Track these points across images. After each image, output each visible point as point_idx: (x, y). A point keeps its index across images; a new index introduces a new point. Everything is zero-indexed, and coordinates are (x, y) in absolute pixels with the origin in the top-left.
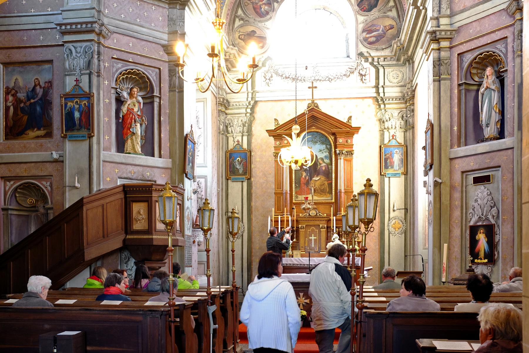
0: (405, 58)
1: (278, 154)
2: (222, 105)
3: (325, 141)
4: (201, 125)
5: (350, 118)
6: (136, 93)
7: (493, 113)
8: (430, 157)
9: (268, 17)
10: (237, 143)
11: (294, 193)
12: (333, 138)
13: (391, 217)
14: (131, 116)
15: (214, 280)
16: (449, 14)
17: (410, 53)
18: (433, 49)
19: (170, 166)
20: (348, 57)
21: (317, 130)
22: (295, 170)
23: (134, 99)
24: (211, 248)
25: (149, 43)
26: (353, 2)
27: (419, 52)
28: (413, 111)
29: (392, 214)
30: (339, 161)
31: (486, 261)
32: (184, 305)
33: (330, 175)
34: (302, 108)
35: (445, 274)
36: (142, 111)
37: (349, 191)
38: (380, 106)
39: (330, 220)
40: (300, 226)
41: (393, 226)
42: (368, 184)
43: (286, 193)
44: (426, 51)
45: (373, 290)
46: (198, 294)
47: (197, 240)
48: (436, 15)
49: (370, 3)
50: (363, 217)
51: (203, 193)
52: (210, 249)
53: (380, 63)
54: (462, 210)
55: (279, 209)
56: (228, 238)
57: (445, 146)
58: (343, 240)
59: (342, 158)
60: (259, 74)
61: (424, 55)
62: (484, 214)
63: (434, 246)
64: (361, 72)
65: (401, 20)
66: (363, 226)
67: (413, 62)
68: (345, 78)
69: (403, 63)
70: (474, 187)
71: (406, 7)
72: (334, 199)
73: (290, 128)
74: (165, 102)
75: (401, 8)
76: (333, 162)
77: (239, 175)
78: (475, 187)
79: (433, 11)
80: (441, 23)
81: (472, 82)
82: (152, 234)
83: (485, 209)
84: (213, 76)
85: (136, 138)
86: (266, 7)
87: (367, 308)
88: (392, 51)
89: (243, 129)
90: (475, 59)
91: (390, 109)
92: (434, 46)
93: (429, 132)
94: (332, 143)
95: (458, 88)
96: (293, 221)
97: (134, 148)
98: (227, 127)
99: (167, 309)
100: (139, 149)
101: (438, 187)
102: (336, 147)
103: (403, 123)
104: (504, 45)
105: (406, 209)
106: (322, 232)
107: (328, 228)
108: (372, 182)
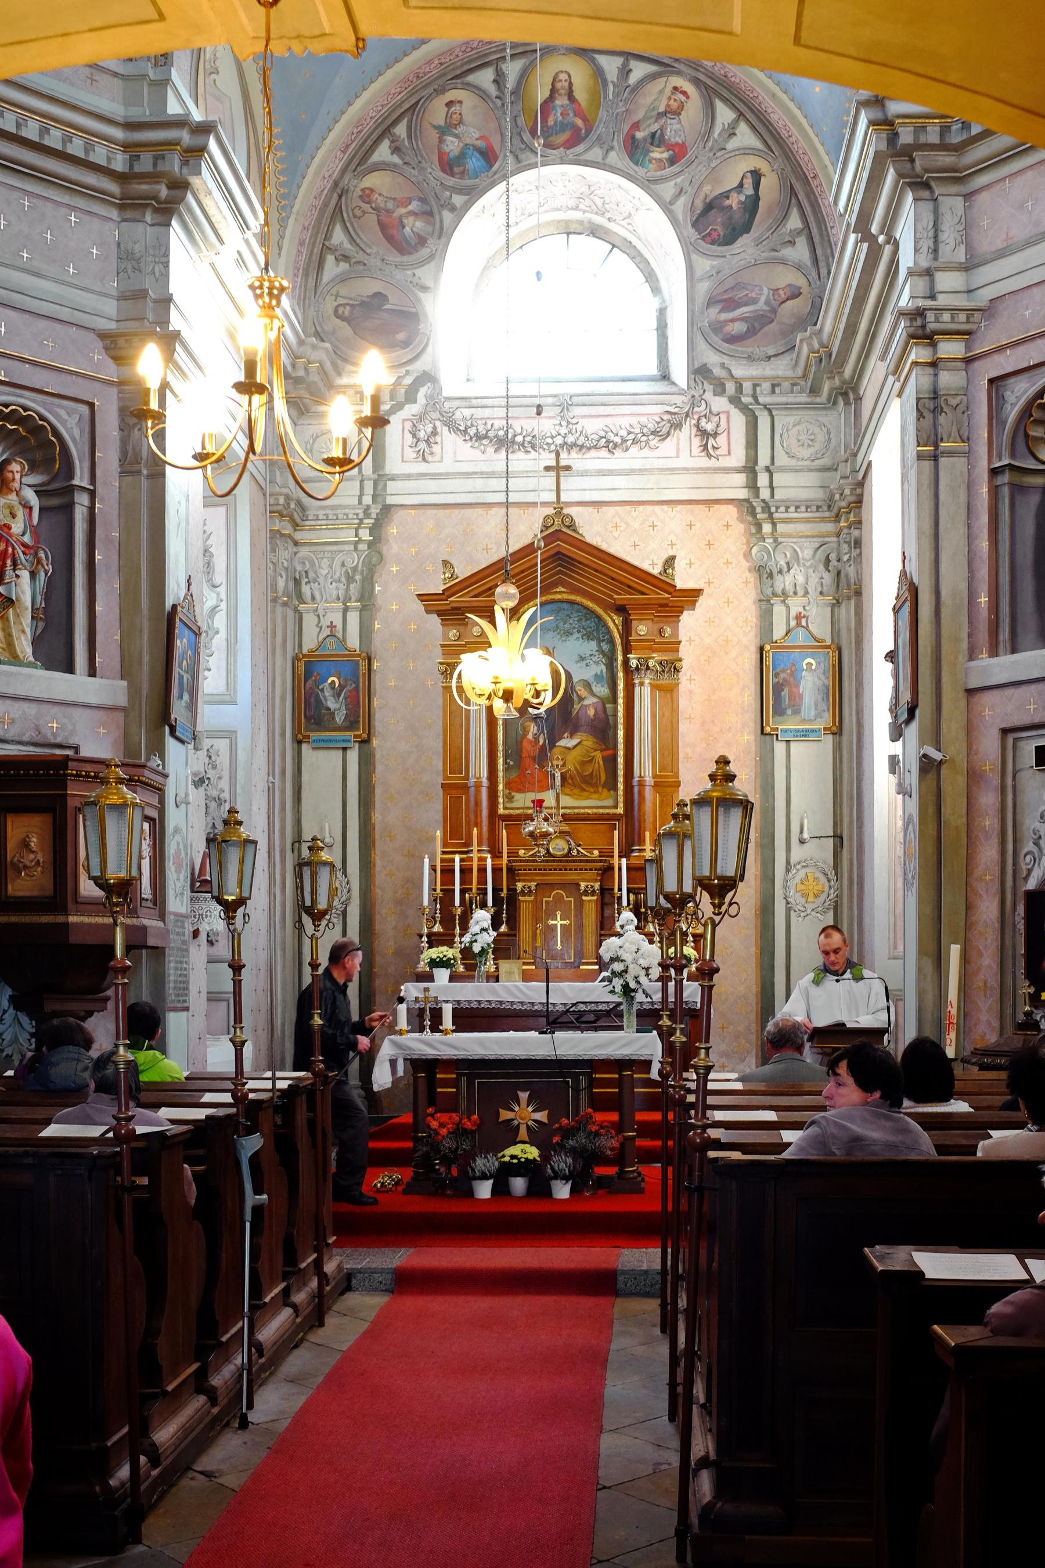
1: (453, 666)
2: (282, 516)
3: (597, 631)
4: (220, 577)
5: (670, 561)
6: (17, 476)
8: (908, 685)
9: (425, 252)
10: (328, 632)
11: (501, 787)
12: (618, 620)
13: (793, 862)
15: (257, 1050)
16: (963, 260)
18: (915, 364)
19: (122, 700)
21: (573, 597)
22: (505, 721)
23: (13, 497)
24: (245, 959)
25: (58, 326)
26: (681, 218)
27: (876, 370)
28: (858, 543)
29: (798, 853)
30: (637, 689)
32: (162, 1134)
33: (611, 733)
34: (527, 530)
35: (952, 1035)
36: (35, 532)
37: (667, 784)
38: (759, 526)
39: (611, 868)
41: (801, 887)
42: (723, 774)
43: (478, 785)
44: (897, 367)
45: (738, 1086)
46: (208, 1098)
47: (204, 928)
48: (925, 263)
49: (730, 218)
50: (706, 872)
51: (224, 784)
52: (244, 961)
53: (760, 400)
55: (456, 833)
56: (299, 925)
57: (954, 650)
58: (651, 928)
59: (647, 681)
60: (395, 433)
61: (891, 379)
63: (921, 952)
65: (823, 271)
66: (705, 900)
67: (859, 399)
68: (654, 441)
69: (829, 400)
71: (837, 233)
72: (621, 805)
73: (490, 590)
74: (107, 506)
75: (821, 235)
76: (621, 694)
77: (334, 730)
81: (1032, 465)
82: (65, 912)
84: (251, 448)
86: (419, 224)
87: (718, 1145)
88: (796, 364)
89: (348, 589)
91: (790, 536)
92: (918, 353)
93: (907, 608)
94: (616, 635)
95: (990, 481)
96: (497, 870)
98: (297, 582)
99: (110, 1150)
100: (25, 647)
101: (931, 776)
102: (627, 649)
103: (828, 578)
105: (838, 838)
106: (586, 906)
108: (732, 768)
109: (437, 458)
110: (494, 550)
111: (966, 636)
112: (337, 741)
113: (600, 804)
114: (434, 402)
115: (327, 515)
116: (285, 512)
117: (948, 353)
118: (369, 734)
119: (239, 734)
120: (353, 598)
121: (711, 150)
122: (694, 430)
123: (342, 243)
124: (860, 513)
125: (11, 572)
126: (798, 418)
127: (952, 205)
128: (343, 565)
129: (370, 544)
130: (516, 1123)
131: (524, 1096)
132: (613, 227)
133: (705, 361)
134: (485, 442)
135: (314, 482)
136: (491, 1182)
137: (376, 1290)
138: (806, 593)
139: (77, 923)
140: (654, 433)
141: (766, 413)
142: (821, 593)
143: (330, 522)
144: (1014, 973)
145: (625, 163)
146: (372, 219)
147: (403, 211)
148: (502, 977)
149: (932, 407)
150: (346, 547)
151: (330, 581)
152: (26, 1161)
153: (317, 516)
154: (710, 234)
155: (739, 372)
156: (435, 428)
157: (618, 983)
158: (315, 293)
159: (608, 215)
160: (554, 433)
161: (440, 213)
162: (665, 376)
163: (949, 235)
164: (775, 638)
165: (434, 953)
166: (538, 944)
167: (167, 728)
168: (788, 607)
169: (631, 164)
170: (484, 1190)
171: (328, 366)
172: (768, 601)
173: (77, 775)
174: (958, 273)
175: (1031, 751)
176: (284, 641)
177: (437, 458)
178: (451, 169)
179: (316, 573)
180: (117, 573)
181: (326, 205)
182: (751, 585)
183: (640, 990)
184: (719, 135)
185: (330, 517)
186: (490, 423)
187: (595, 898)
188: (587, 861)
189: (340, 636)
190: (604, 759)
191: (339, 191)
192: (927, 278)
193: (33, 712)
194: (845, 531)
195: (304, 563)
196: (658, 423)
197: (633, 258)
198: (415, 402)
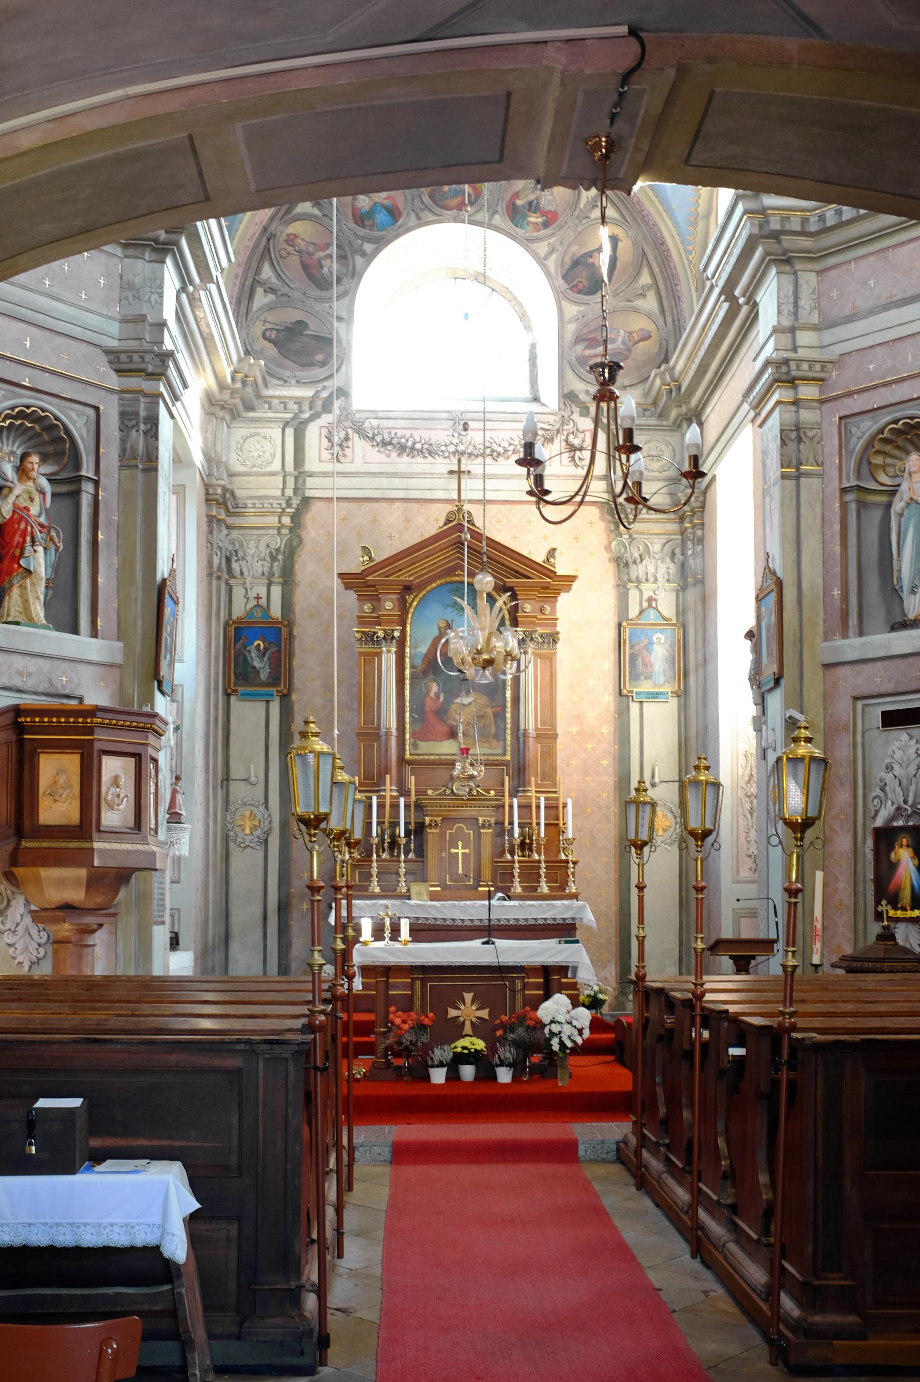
2: (218, 504)
5: (552, 552)
6: (36, 467)
10: (253, 603)
11: (408, 736)
14: (23, 526)
16: (817, 322)
17: (694, 401)
19: (119, 659)
20: (536, 399)
23: (30, 483)
25: (72, 342)
26: (553, 271)
28: (701, 541)
34: (430, 522)
40: (427, 819)
43: (388, 734)
48: (787, 322)
54: (855, 789)
59: (530, 651)
62: (910, 802)
64: (571, 438)
69: (674, 424)
70: (884, 735)
72: (509, 753)
78: (886, 733)
79: (779, 312)
80: (799, 342)
81: (873, 485)
90: (881, 431)
93: (773, 598)
97: (26, 608)
98: (228, 560)
100: (38, 611)
103: (673, 568)
109: (349, 459)
111: (821, 621)
112: (262, 695)
113: (490, 752)
114: (346, 413)
115: (271, 504)
117: (805, 395)
119: (185, 687)
120: (277, 575)
121: (577, 217)
122: (564, 444)
123: (269, 278)
126: (648, 437)
127: (809, 279)
128: (268, 546)
130: (462, 1019)
131: (468, 997)
133: (573, 388)
134: (389, 447)
135: (244, 476)
136: (445, 1069)
142: (668, 581)
143: (257, 510)
144: (865, 895)
145: (507, 225)
146: (295, 260)
147: (322, 254)
151: (256, 559)
152: (238, 1047)
154: (576, 285)
156: (347, 434)
158: (246, 318)
160: (448, 442)
161: (353, 258)
163: (805, 302)
164: (631, 616)
167: (156, 683)
168: (641, 592)
169: (512, 226)
170: (438, 1076)
171: (260, 381)
172: (625, 586)
174: (813, 333)
177: (349, 459)
178: (362, 221)
179: (244, 552)
180: (115, 550)
181: (256, 246)
182: (611, 572)
184: (585, 206)
185: (257, 506)
186: (393, 432)
188: (485, 800)
191: (268, 235)
192: (789, 335)
193: (47, 667)
195: (234, 544)
198: (330, 412)
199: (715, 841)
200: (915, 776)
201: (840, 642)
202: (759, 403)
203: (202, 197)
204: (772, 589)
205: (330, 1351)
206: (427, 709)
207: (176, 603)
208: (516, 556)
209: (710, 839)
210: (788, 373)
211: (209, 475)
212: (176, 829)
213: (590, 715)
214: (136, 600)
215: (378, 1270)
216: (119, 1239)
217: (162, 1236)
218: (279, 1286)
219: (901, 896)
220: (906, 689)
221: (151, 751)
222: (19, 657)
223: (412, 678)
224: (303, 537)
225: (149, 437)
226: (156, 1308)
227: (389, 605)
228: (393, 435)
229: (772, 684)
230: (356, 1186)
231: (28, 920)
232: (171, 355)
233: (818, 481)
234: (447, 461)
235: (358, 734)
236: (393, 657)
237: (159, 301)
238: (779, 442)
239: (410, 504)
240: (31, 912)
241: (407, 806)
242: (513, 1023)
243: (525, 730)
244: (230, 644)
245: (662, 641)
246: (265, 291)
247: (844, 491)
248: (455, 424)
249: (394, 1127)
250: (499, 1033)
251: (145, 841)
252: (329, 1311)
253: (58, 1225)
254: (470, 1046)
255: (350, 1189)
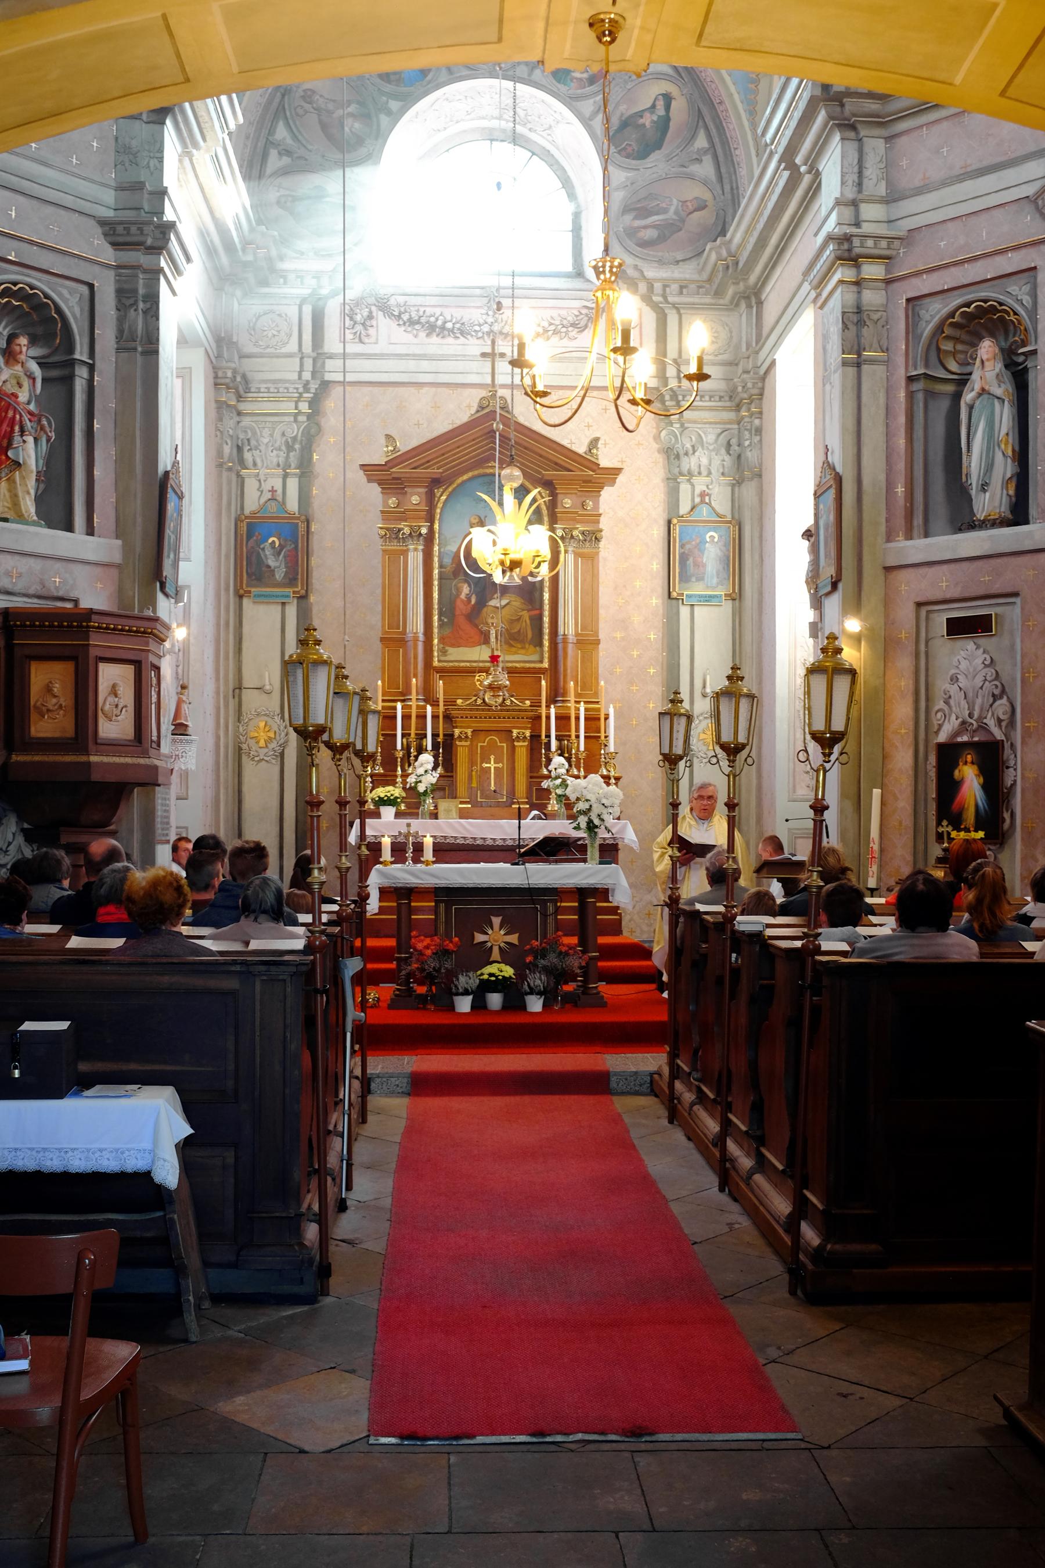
0: (741, 293)
5: (594, 443)
7: (999, 456)
11: (436, 641)
14: (10, 414)
16: (884, 194)
17: (753, 279)
19: (117, 558)
23: (19, 367)
25: (62, 212)
28: (759, 431)
31: (981, 834)
33: (537, 595)
34: (459, 411)
35: (874, 868)
36: (38, 400)
39: (539, 717)
40: (457, 732)
48: (850, 194)
53: (670, 299)
59: (570, 549)
62: (976, 716)
67: (760, 303)
68: (573, 333)
69: (731, 303)
70: (949, 644)
72: (546, 660)
75: (725, 154)
79: (843, 183)
81: (942, 374)
83: (979, 701)
85: (23, 478)
86: (357, 125)
89: (287, 457)
90: (952, 315)
91: (695, 422)
93: (831, 494)
98: (239, 449)
100: (29, 506)
104: (1026, 288)
107: (535, 737)
109: (373, 340)
110: (425, 426)
111: (884, 520)
112: (277, 596)
113: (526, 658)
116: (231, 385)
118: (307, 591)
120: (293, 466)
123: (284, 139)
124: (761, 404)
125: (19, 438)
127: (875, 146)
128: (283, 434)
129: (309, 417)
130: (489, 944)
131: (496, 921)
132: (533, 136)
134: (417, 327)
136: (471, 997)
137: (393, 1093)
138: (709, 473)
139: (97, 763)
140: (573, 325)
141: (674, 311)
142: (723, 474)
144: (926, 814)
147: (340, 112)
148: (441, 814)
149: (855, 321)
150: (286, 419)
152: (233, 968)
153: (259, 388)
154: (625, 149)
155: (651, 273)
156: (371, 312)
157: (583, 821)
159: (529, 126)
160: (482, 321)
162: (579, 274)
163: (872, 172)
164: (681, 513)
165: (381, 792)
166: (474, 785)
168: (693, 485)
170: (464, 1005)
173: (99, 628)
175: (942, 623)
176: (229, 504)
177: (373, 340)
179: (257, 441)
181: (270, 102)
183: (603, 827)
186: (422, 309)
187: (526, 744)
189: (280, 499)
190: (531, 618)
192: (852, 208)
194: (746, 420)
195: (246, 432)
196: (577, 316)
197: (550, 166)
199: (749, 756)
200: (981, 688)
201: (901, 543)
202: (821, 283)
203: (181, 79)
204: (832, 485)
205: (332, 1281)
206: (458, 612)
207: (181, 497)
208: (555, 446)
209: (744, 754)
210: (849, 250)
211: (219, 356)
212: (181, 741)
213: (636, 619)
214: (135, 495)
215: (388, 1202)
216: (109, 1164)
217: (153, 1161)
218: (277, 1214)
219: (964, 816)
220: (973, 594)
221: (152, 658)
222: (8, 557)
223: (440, 578)
224: (322, 424)
225: (149, 317)
226: (149, 1235)
227: (415, 499)
228: (421, 313)
229: (829, 588)
230: (370, 1118)
231: (20, 839)
232: (172, 226)
233: (883, 368)
234: (480, 342)
235: (382, 639)
236: (420, 555)
237: (158, 165)
238: (840, 325)
239: (439, 389)
240: (23, 830)
241: (435, 717)
242: (544, 948)
243: (564, 635)
244: (242, 540)
245: (716, 540)
246: (280, 153)
247: (910, 379)
248: (489, 301)
249: (414, 1058)
250: (529, 959)
251: (145, 754)
252: (333, 1243)
253: (45, 1150)
254: (498, 973)
255: (364, 1121)
